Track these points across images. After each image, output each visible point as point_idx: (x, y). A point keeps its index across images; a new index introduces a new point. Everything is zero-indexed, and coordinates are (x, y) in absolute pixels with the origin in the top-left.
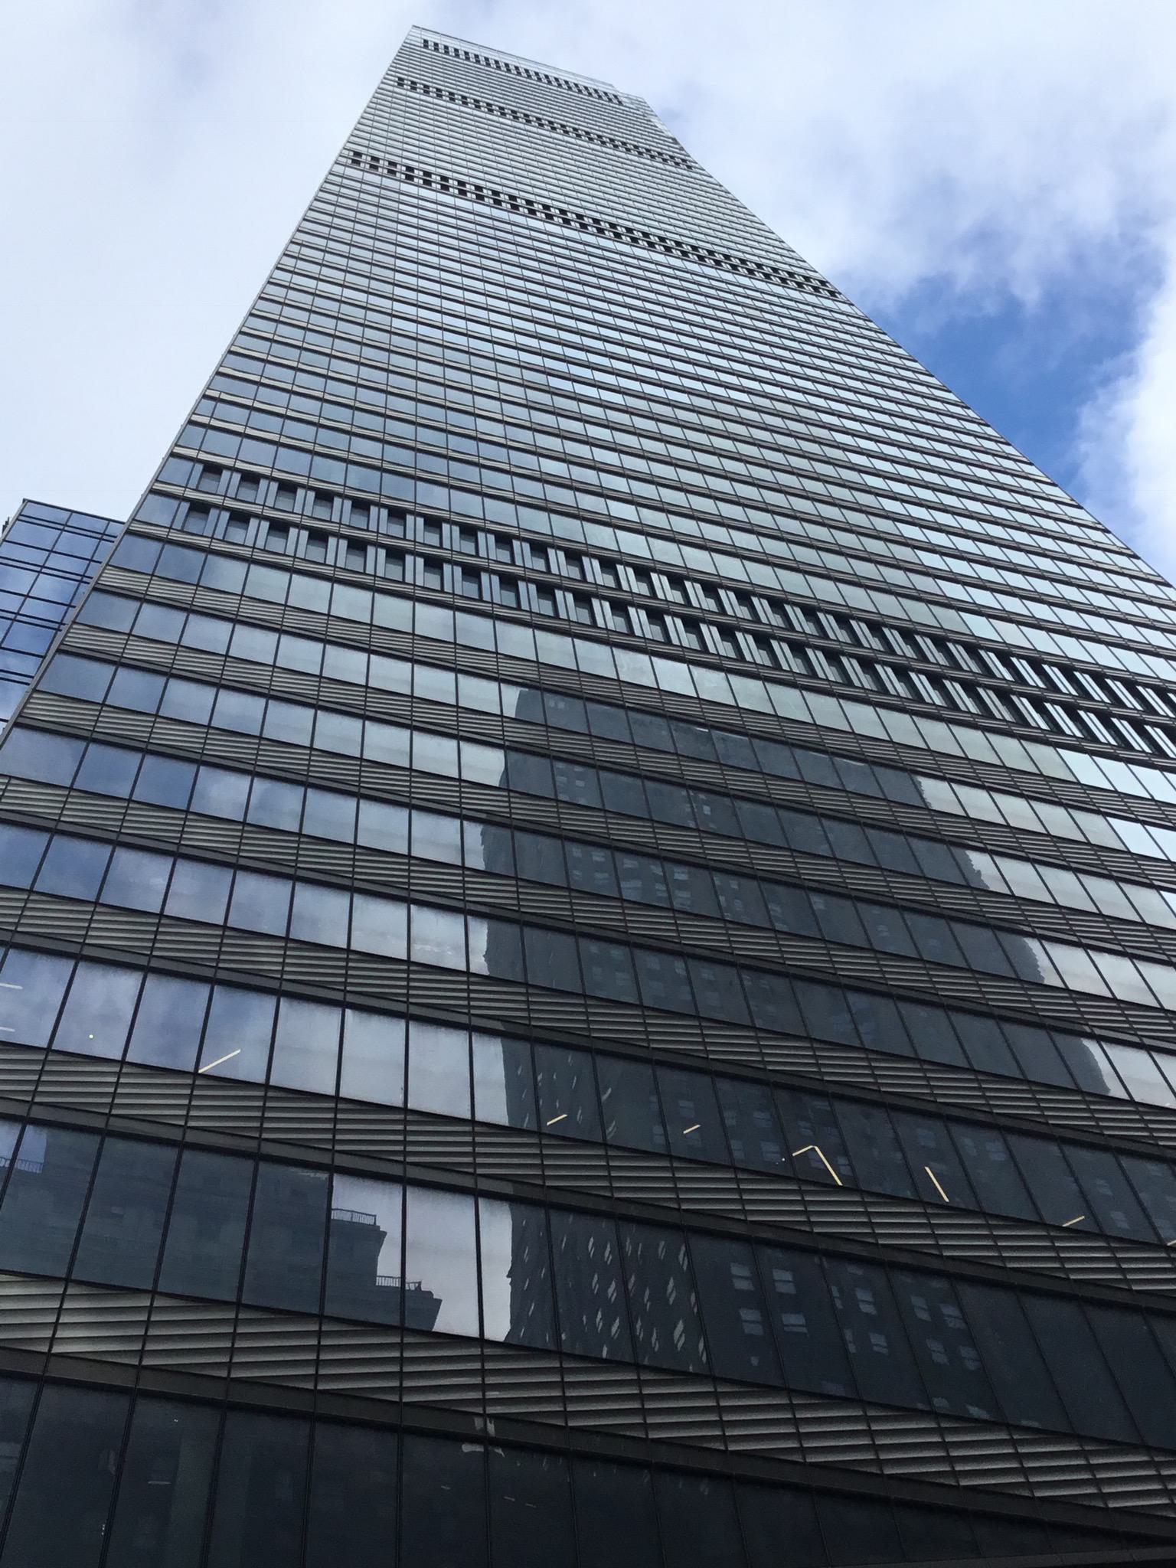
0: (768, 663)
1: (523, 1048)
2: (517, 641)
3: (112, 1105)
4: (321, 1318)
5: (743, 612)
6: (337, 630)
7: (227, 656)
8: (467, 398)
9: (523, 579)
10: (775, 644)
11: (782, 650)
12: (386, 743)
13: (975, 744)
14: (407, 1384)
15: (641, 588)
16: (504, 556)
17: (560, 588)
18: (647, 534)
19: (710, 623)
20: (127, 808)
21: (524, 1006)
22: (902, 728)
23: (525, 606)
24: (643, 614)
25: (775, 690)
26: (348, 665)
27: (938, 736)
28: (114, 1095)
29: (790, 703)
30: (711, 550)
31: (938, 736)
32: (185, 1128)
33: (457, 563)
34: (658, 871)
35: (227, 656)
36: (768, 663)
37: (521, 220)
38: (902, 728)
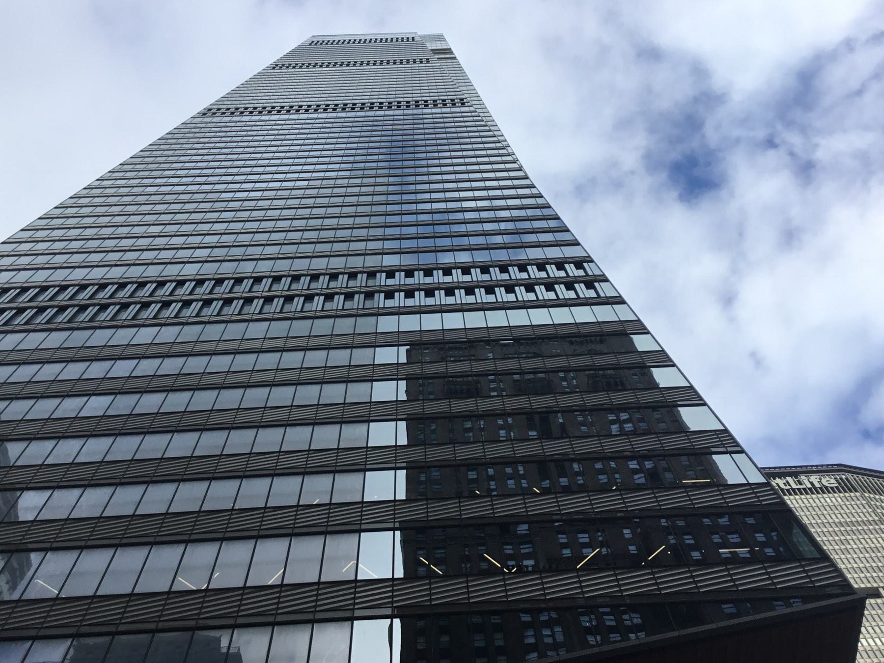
12: (177, 402)
26: (49, 372)
37: (458, 110)
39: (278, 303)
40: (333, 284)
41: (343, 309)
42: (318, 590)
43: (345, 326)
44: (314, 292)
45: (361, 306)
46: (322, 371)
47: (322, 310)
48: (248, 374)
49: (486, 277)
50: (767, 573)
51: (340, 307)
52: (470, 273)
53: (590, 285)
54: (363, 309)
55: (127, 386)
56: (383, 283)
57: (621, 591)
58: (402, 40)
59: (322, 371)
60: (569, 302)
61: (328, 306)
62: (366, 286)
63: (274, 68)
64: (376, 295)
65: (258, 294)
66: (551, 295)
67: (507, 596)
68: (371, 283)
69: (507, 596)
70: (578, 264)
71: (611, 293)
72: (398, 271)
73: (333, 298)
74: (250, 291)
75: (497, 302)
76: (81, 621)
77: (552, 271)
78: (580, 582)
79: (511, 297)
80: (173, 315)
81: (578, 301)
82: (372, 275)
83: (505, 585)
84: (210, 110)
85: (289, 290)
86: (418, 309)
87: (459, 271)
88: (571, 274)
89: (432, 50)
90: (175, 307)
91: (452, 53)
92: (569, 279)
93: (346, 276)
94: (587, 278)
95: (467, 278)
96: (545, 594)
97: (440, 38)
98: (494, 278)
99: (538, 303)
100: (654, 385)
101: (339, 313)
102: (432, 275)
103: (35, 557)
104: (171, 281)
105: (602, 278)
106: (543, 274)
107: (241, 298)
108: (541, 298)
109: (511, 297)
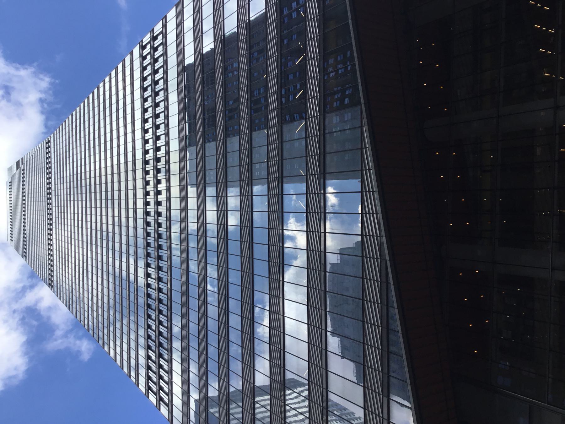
0: (161, 35)
1: (285, 179)
2: (175, 192)
4: (362, 149)
5: (149, 57)
6: (184, 219)
13: (172, 50)
14: (375, 212)
15: (149, 68)
25: (169, 54)
27: (172, 61)
31: (172, 61)
32: (320, 213)
33: (157, 165)
36: (161, 35)
38: (173, 74)
39: (162, 307)
40: (153, 256)
41: (167, 262)
42: (311, 288)
43: (177, 297)
44: (157, 276)
45: (166, 252)
46: (200, 263)
47: (167, 273)
48: (200, 328)
49: (151, 162)
50: (311, 59)
51: (166, 263)
52: (149, 171)
54: (167, 251)
55: (204, 365)
56: (153, 228)
57: (317, 76)
58: (11, 219)
59: (200, 237)
60: (167, 139)
61: (165, 269)
62: (155, 258)
63: (26, 257)
64: (160, 232)
65: (157, 306)
66: (163, 137)
67: (317, 155)
68: (153, 235)
69: (317, 174)
72: (146, 199)
73: (160, 245)
74: (155, 300)
75: (165, 145)
76: (320, 406)
77: (149, 136)
78: (312, 175)
79: (163, 160)
80: (166, 341)
81: (166, 100)
82: (148, 245)
83: (312, 175)
84: (50, 284)
85: (155, 290)
86: (168, 199)
87: (147, 176)
88: (151, 115)
89: (17, 169)
90: (162, 340)
91: (19, 161)
93: (148, 248)
94: (153, 96)
95: (152, 183)
96: (317, 135)
97: (10, 169)
98: (152, 147)
99: (167, 145)
100: (213, 50)
101: (169, 252)
102: (149, 181)
103: (289, 376)
104: (147, 332)
105: (152, 32)
106: (151, 141)
107: (158, 305)
108: (164, 132)
109: (163, 160)
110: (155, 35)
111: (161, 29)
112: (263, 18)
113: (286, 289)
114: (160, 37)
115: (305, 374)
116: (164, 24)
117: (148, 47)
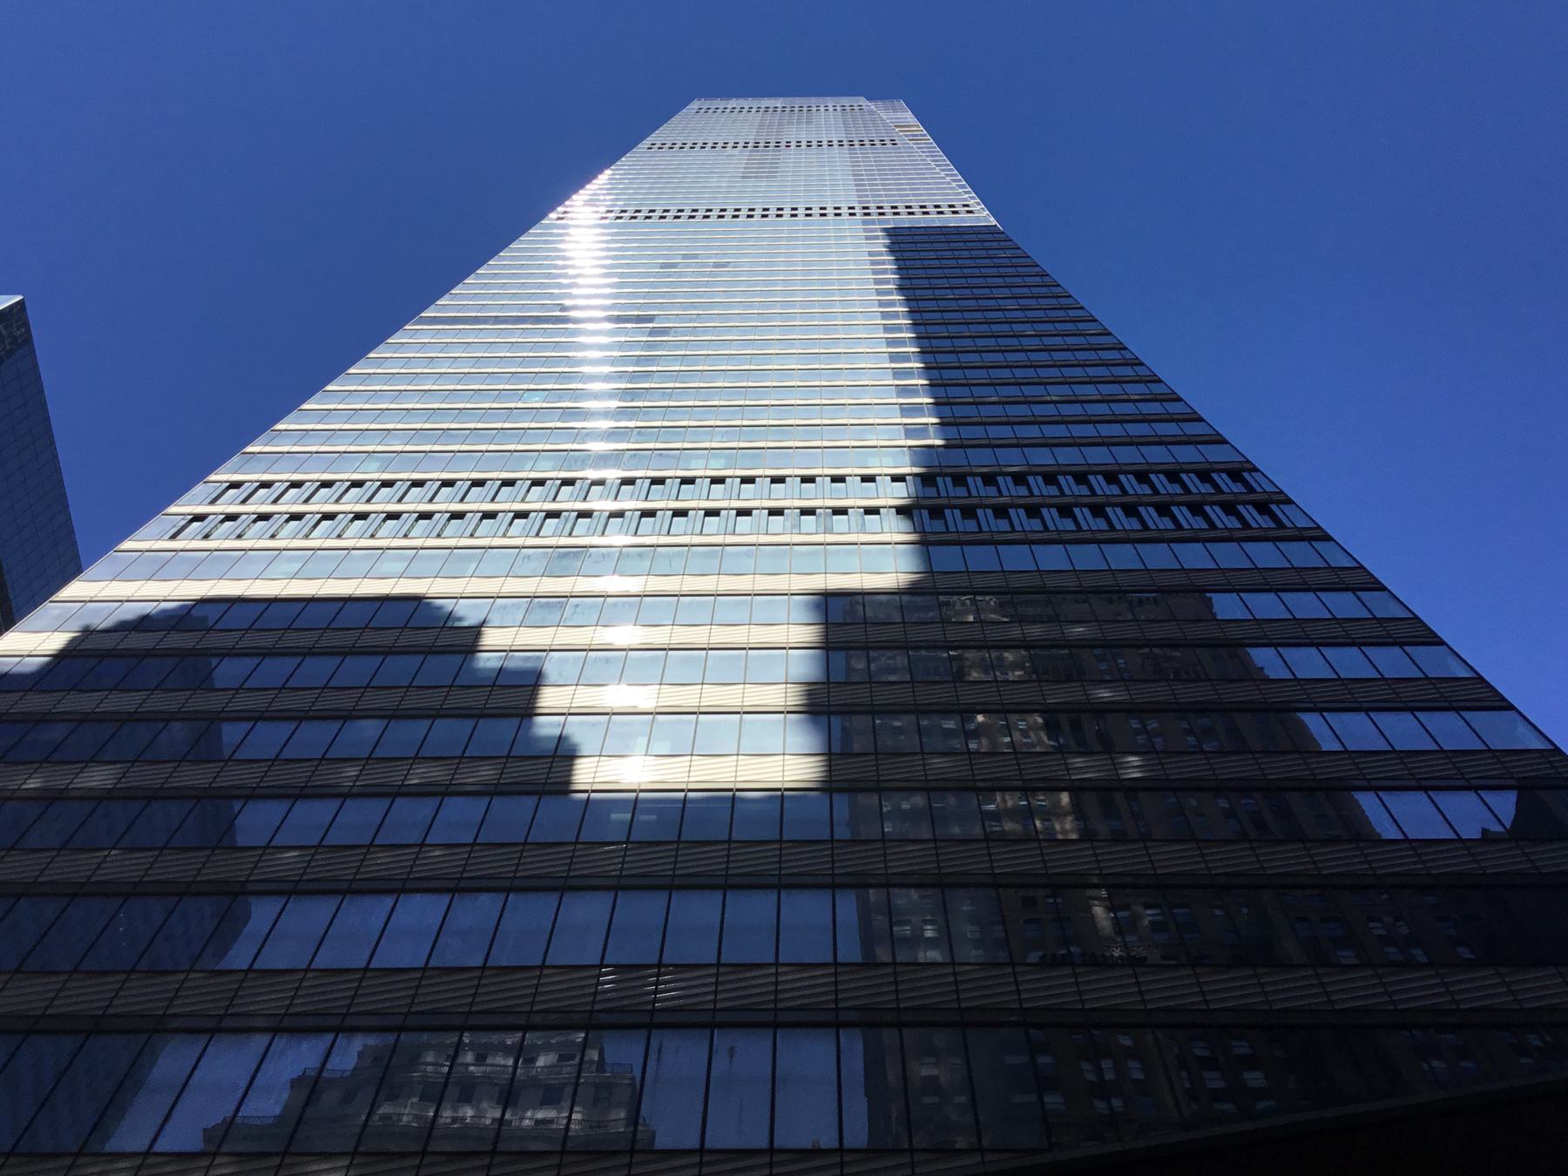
3: (776, 1001)
7: (832, 841)
8: (1006, 327)
9: (1043, 506)
10: (1241, 508)
11: (1215, 513)
16: (1023, 491)
17: (1077, 505)
18: (1108, 445)
19: (1179, 504)
20: (717, 975)
21: (1147, 997)
22: (1194, 556)
23: (1051, 527)
24: (1119, 510)
25: (1214, 548)
28: (776, 983)
29: (1122, 557)
30: (1166, 444)
34: (1135, 725)
35: (832, 841)
38: (1194, 556)
53: (1263, 508)
70: (1236, 474)
71: (1301, 523)
92: (940, 501)
105: (1279, 497)
110: (1273, 507)
111: (1289, 524)
112: (1359, 833)
113: (485, 898)
114: (1265, 522)
115: (274, 958)
116: (1099, 536)
117: (1238, 488)
